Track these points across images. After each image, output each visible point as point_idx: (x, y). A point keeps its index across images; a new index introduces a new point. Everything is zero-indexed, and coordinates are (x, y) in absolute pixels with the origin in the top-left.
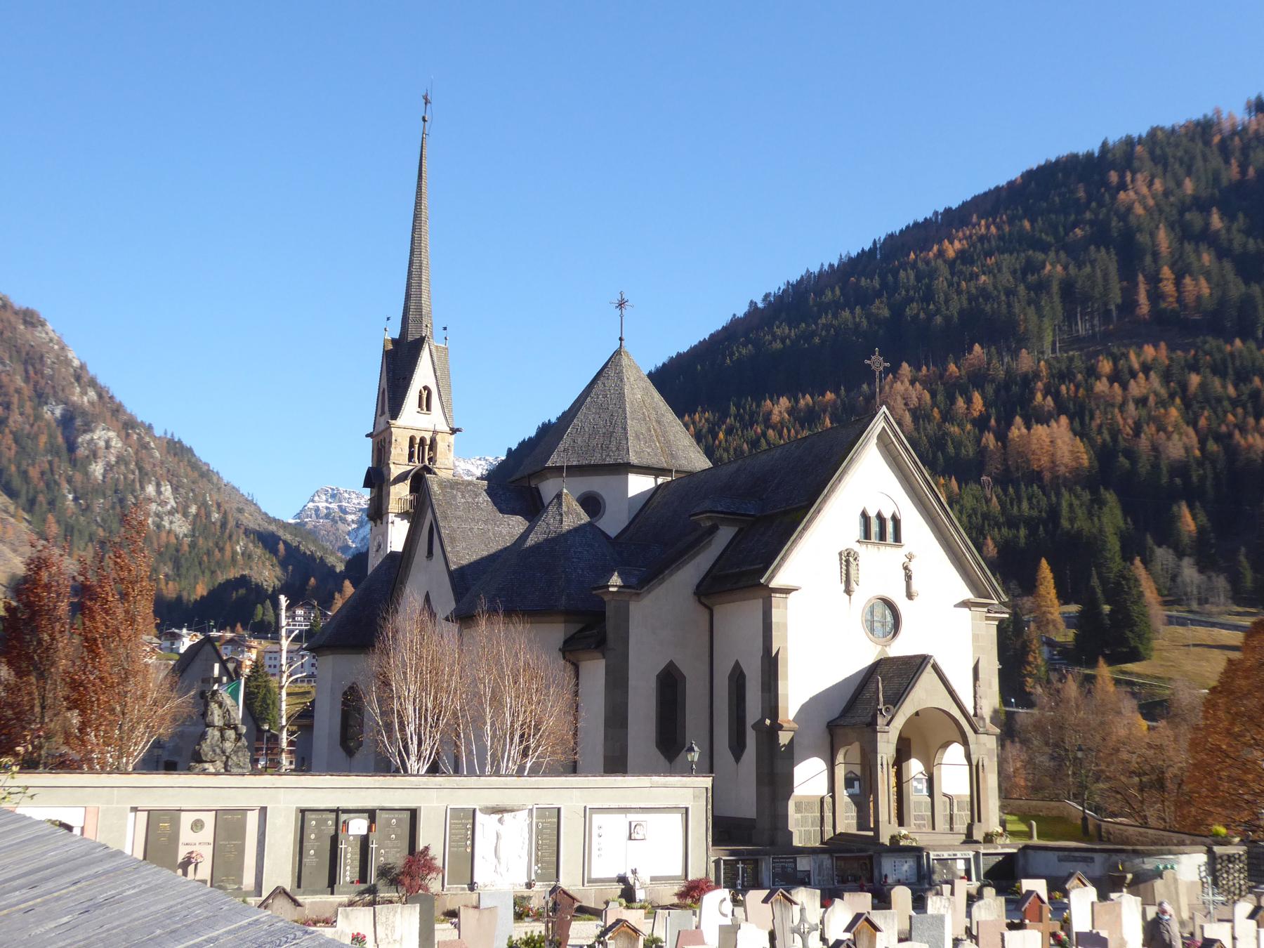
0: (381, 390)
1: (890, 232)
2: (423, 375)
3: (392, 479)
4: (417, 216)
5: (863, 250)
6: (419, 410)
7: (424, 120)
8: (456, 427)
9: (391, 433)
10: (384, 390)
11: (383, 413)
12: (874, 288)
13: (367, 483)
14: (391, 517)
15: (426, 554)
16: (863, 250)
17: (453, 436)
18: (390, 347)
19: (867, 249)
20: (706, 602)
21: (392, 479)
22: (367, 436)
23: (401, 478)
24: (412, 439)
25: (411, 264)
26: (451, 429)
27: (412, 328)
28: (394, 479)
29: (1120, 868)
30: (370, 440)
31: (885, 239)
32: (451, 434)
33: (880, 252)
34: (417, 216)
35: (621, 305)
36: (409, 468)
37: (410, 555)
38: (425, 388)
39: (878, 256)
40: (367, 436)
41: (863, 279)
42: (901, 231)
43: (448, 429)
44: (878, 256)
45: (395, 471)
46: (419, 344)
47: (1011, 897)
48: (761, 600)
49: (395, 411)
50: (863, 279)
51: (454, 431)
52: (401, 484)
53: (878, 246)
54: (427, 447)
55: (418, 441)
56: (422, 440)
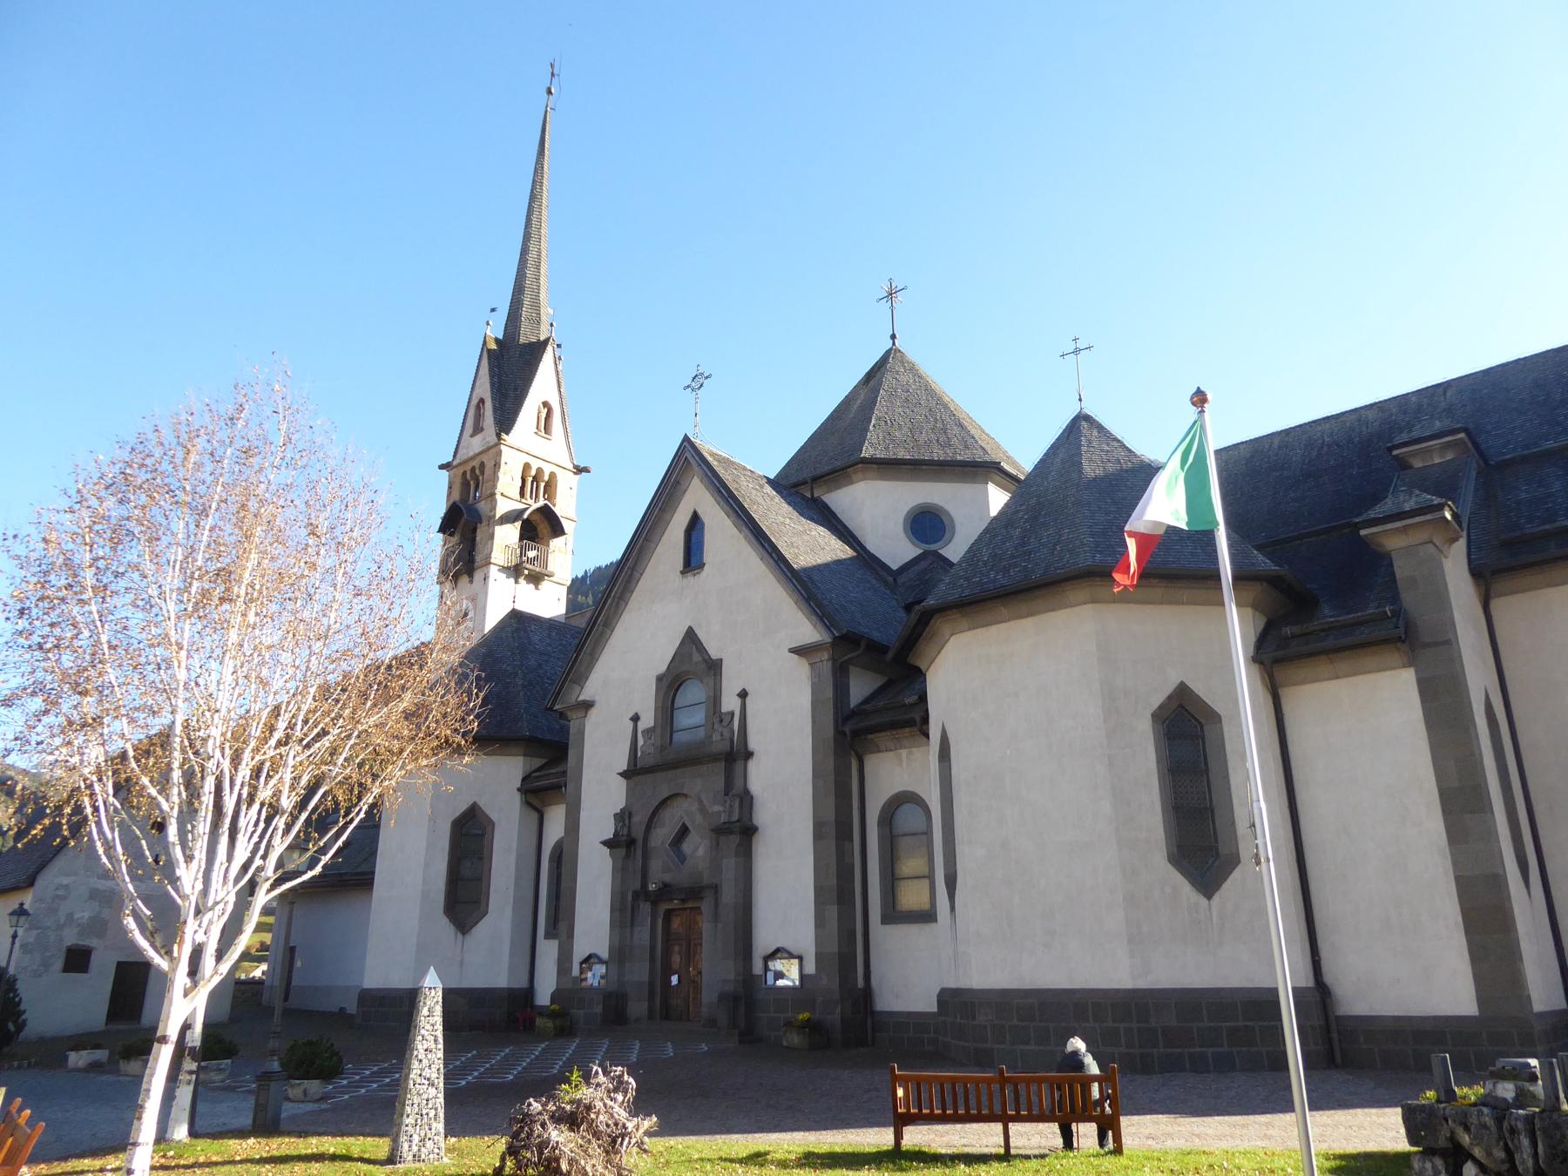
0: (475, 402)
1: (598, 566)
2: (543, 386)
3: (498, 516)
4: (534, 197)
7: (549, 92)
9: (499, 453)
10: (482, 401)
11: (478, 429)
13: (447, 526)
15: (681, 567)
17: (577, 477)
19: (580, 576)
20: (535, 802)
21: (498, 516)
22: (442, 467)
23: (509, 518)
24: (527, 467)
25: (524, 251)
26: (576, 467)
28: (501, 517)
30: (445, 473)
34: (534, 197)
35: (891, 295)
38: (545, 404)
39: (588, 582)
40: (442, 467)
42: (607, 566)
43: (571, 467)
44: (588, 582)
45: (503, 507)
46: (536, 350)
48: (564, 806)
49: (506, 421)
51: (579, 470)
52: (509, 526)
55: (533, 472)
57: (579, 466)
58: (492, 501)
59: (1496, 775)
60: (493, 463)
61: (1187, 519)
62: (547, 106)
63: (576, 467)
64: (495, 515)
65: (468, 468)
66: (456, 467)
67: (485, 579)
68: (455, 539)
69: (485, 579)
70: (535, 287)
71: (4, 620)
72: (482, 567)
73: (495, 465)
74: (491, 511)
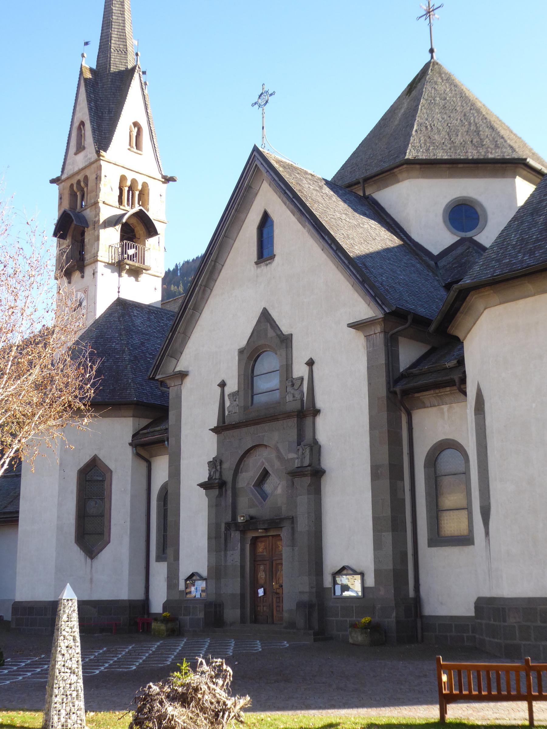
0: (76, 124)
3: (101, 222)
5: (169, 270)
6: (129, 147)
8: (169, 176)
10: (82, 123)
11: (80, 148)
12: (179, 292)
14: (100, 267)
15: (255, 259)
16: (169, 270)
18: (88, 75)
19: (171, 269)
21: (101, 222)
22: (53, 181)
23: (111, 222)
24: (123, 179)
26: (164, 177)
27: (115, 58)
29: (444, 678)
30: (55, 187)
31: (183, 264)
32: (164, 183)
33: (180, 272)
36: (120, 212)
37: (214, 267)
38: (136, 124)
39: (179, 274)
40: (53, 181)
41: (172, 286)
42: (193, 260)
44: (179, 274)
47: (12, 681)
50: (172, 286)
51: (167, 180)
53: (179, 268)
54: (137, 193)
55: (129, 183)
56: (134, 181)
57: (167, 176)
58: (96, 208)
63: (164, 177)
64: (99, 220)
67: (94, 274)
69: (94, 274)
73: (96, 178)
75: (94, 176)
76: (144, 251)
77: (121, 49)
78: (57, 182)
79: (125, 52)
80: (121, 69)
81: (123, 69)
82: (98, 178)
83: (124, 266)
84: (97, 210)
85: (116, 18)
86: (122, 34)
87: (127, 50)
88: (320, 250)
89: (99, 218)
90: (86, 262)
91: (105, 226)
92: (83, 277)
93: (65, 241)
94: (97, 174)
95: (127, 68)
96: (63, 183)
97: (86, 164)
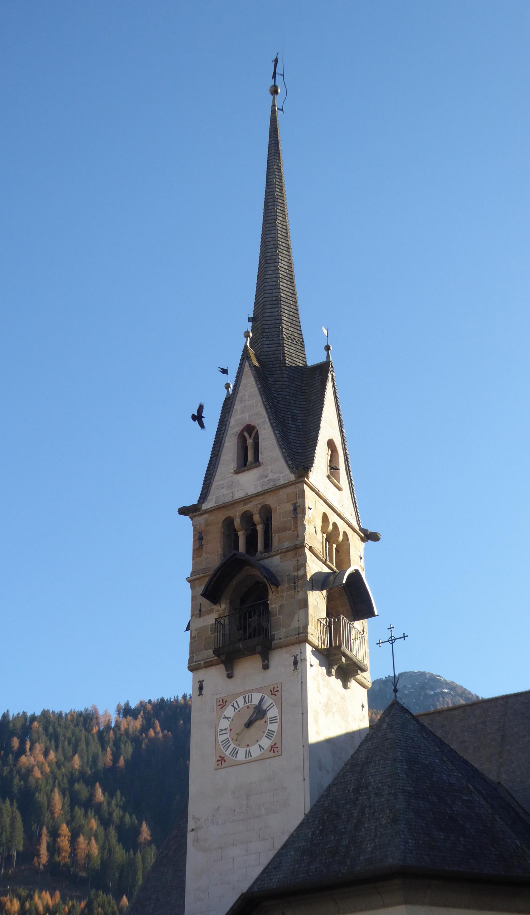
8: (371, 530)
22: (183, 511)
30: (186, 521)
40: (183, 511)
57: (367, 530)
58: (296, 556)
59: (309, 796)
60: (292, 508)
61: (318, 661)
62: (274, 105)
63: (363, 531)
64: (305, 575)
65: (236, 514)
66: (206, 512)
67: (295, 663)
68: (223, 608)
69: (295, 663)
70: (292, 303)
71: (249, 744)
72: (286, 646)
73: (295, 510)
74: (298, 569)
75: (289, 507)
76: (350, 640)
77: (297, 339)
78: (193, 512)
79: (301, 343)
80: (298, 364)
81: (301, 365)
82: (299, 510)
83: (338, 656)
84: (301, 559)
85: (285, 296)
86: (294, 319)
87: (303, 341)
88: (99, 712)
89: (306, 572)
90: (274, 642)
91: (313, 586)
92: (266, 667)
93: (215, 607)
94: (294, 504)
95: (306, 365)
96: (206, 516)
97: (260, 489)
